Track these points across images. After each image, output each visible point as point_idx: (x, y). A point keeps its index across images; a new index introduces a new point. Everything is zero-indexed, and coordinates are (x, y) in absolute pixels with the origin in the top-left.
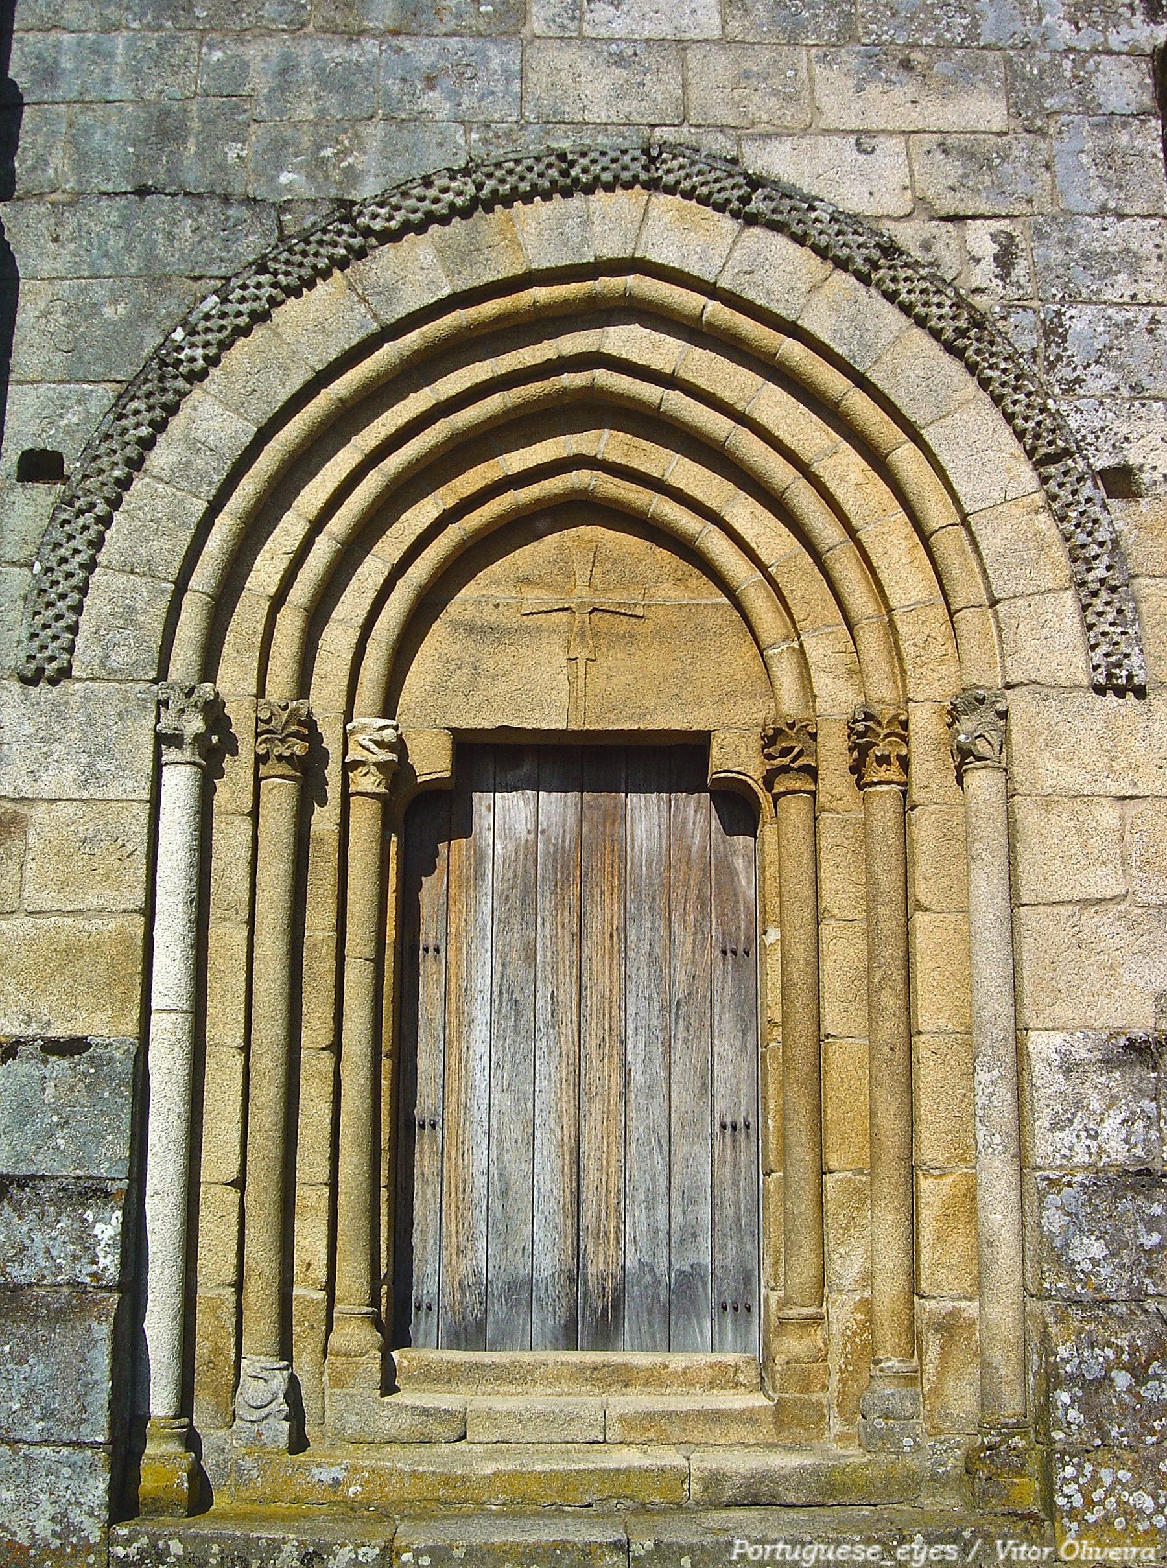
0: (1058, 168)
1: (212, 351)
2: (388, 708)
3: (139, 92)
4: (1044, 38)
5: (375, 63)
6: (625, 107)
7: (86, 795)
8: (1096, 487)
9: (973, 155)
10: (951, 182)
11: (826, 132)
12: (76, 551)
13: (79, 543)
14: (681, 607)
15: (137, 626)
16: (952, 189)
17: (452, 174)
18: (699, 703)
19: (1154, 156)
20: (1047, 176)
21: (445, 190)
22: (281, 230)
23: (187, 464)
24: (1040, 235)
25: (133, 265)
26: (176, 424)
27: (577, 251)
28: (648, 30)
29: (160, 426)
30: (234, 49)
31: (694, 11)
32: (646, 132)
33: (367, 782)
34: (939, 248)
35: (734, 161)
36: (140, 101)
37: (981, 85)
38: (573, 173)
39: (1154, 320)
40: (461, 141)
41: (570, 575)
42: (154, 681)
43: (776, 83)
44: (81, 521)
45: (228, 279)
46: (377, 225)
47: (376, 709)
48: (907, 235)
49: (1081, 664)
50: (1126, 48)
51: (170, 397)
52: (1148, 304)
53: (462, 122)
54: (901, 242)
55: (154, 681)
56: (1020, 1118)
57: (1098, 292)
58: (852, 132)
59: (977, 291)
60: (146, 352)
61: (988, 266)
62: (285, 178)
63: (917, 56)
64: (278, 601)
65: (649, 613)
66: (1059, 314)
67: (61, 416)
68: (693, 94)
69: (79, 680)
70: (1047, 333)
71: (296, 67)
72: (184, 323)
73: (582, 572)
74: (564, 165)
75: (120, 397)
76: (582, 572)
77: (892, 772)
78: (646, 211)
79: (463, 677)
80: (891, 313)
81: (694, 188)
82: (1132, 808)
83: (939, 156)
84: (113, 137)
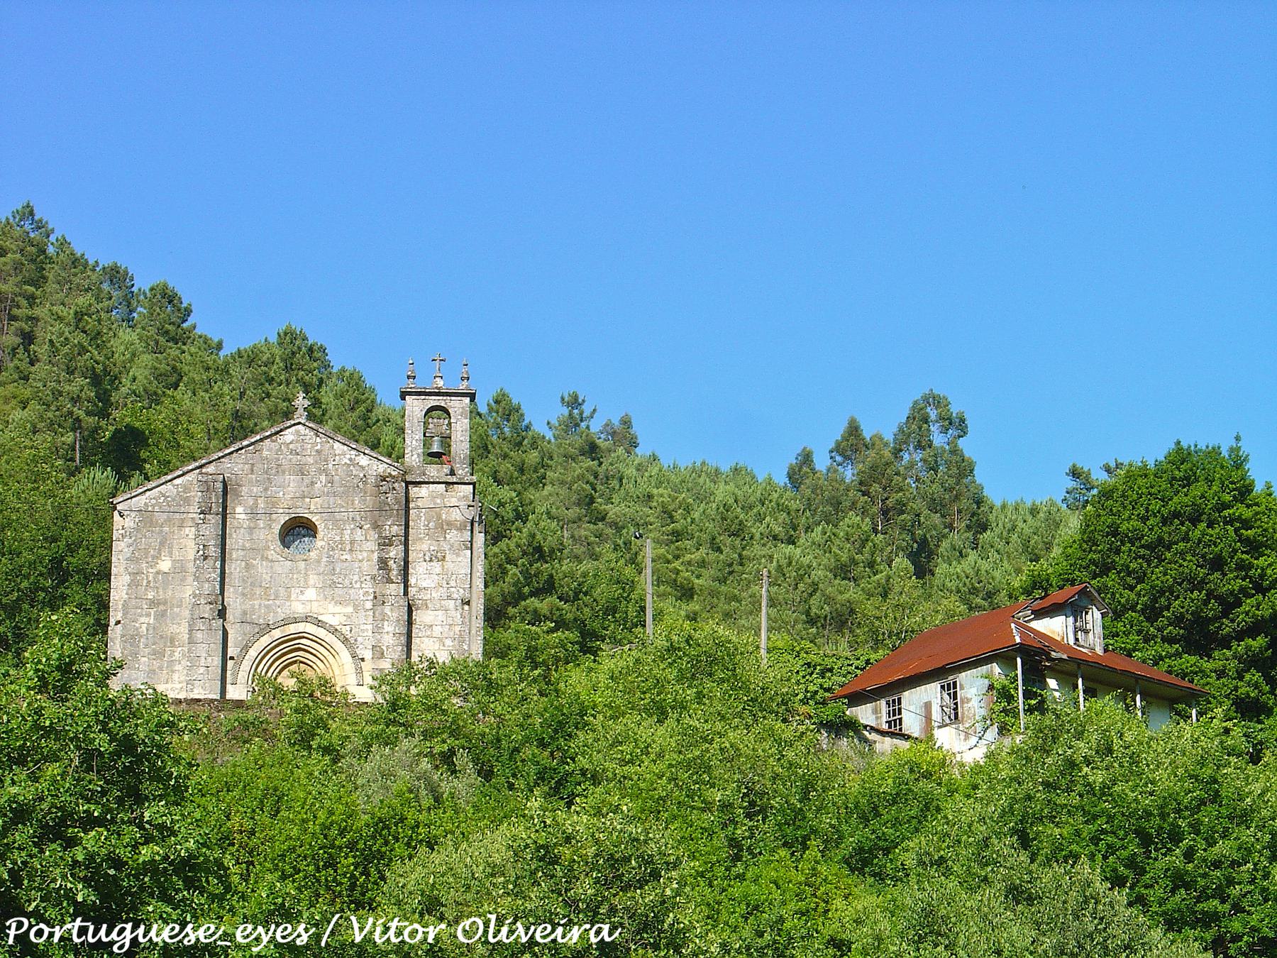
56: (224, 537)
84: (238, 613)
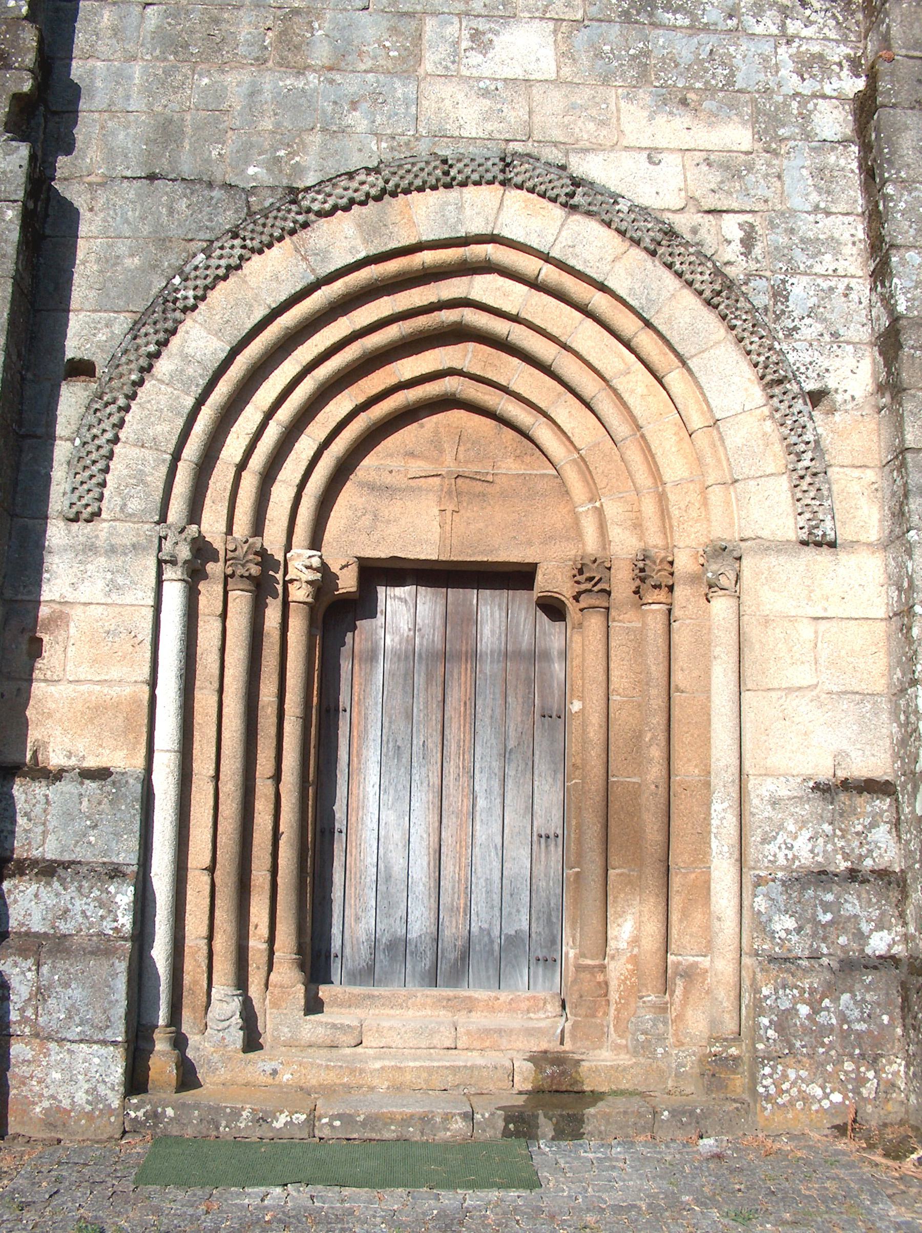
1: (200, 293)
2: (316, 543)
3: (150, 105)
4: (780, 85)
5: (315, 90)
6: (489, 127)
7: (109, 601)
8: (805, 404)
9: (731, 168)
10: (713, 186)
11: (627, 148)
12: (104, 431)
13: (107, 425)
14: (519, 475)
15: (146, 484)
16: (713, 191)
17: (368, 170)
18: (530, 543)
19: (852, 171)
22: (249, 208)
24: (772, 226)
25: (146, 230)
26: (175, 341)
27: (453, 228)
30: (216, 76)
33: (300, 594)
34: (703, 233)
35: (563, 168)
36: (151, 112)
37: (735, 118)
38: (452, 174)
39: (849, 288)
40: (375, 148)
41: (441, 451)
42: (158, 523)
43: (594, 112)
44: (108, 410)
45: (212, 242)
46: (316, 207)
47: (306, 543)
48: (682, 223)
49: (792, 526)
50: (835, 94)
51: (169, 325)
52: (845, 276)
53: (376, 134)
54: (677, 228)
55: (158, 523)
57: (811, 266)
59: (728, 263)
60: (154, 291)
61: (737, 247)
62: (251, 171)
63: (691, 96)
64: (242, 466)
66: (784, 282)
67: (94, 335)
68: (536, 119)
69: (105, 520)
70: (775, 295)
71: (260, 92)
74: (446, 167)
75: (135, 323)
77: (662, 595)
78: (501, 203)
79: (366, 521)
80: (668, 278)
81: (535, 186)
82: (823, 625)
83: (704, 168)
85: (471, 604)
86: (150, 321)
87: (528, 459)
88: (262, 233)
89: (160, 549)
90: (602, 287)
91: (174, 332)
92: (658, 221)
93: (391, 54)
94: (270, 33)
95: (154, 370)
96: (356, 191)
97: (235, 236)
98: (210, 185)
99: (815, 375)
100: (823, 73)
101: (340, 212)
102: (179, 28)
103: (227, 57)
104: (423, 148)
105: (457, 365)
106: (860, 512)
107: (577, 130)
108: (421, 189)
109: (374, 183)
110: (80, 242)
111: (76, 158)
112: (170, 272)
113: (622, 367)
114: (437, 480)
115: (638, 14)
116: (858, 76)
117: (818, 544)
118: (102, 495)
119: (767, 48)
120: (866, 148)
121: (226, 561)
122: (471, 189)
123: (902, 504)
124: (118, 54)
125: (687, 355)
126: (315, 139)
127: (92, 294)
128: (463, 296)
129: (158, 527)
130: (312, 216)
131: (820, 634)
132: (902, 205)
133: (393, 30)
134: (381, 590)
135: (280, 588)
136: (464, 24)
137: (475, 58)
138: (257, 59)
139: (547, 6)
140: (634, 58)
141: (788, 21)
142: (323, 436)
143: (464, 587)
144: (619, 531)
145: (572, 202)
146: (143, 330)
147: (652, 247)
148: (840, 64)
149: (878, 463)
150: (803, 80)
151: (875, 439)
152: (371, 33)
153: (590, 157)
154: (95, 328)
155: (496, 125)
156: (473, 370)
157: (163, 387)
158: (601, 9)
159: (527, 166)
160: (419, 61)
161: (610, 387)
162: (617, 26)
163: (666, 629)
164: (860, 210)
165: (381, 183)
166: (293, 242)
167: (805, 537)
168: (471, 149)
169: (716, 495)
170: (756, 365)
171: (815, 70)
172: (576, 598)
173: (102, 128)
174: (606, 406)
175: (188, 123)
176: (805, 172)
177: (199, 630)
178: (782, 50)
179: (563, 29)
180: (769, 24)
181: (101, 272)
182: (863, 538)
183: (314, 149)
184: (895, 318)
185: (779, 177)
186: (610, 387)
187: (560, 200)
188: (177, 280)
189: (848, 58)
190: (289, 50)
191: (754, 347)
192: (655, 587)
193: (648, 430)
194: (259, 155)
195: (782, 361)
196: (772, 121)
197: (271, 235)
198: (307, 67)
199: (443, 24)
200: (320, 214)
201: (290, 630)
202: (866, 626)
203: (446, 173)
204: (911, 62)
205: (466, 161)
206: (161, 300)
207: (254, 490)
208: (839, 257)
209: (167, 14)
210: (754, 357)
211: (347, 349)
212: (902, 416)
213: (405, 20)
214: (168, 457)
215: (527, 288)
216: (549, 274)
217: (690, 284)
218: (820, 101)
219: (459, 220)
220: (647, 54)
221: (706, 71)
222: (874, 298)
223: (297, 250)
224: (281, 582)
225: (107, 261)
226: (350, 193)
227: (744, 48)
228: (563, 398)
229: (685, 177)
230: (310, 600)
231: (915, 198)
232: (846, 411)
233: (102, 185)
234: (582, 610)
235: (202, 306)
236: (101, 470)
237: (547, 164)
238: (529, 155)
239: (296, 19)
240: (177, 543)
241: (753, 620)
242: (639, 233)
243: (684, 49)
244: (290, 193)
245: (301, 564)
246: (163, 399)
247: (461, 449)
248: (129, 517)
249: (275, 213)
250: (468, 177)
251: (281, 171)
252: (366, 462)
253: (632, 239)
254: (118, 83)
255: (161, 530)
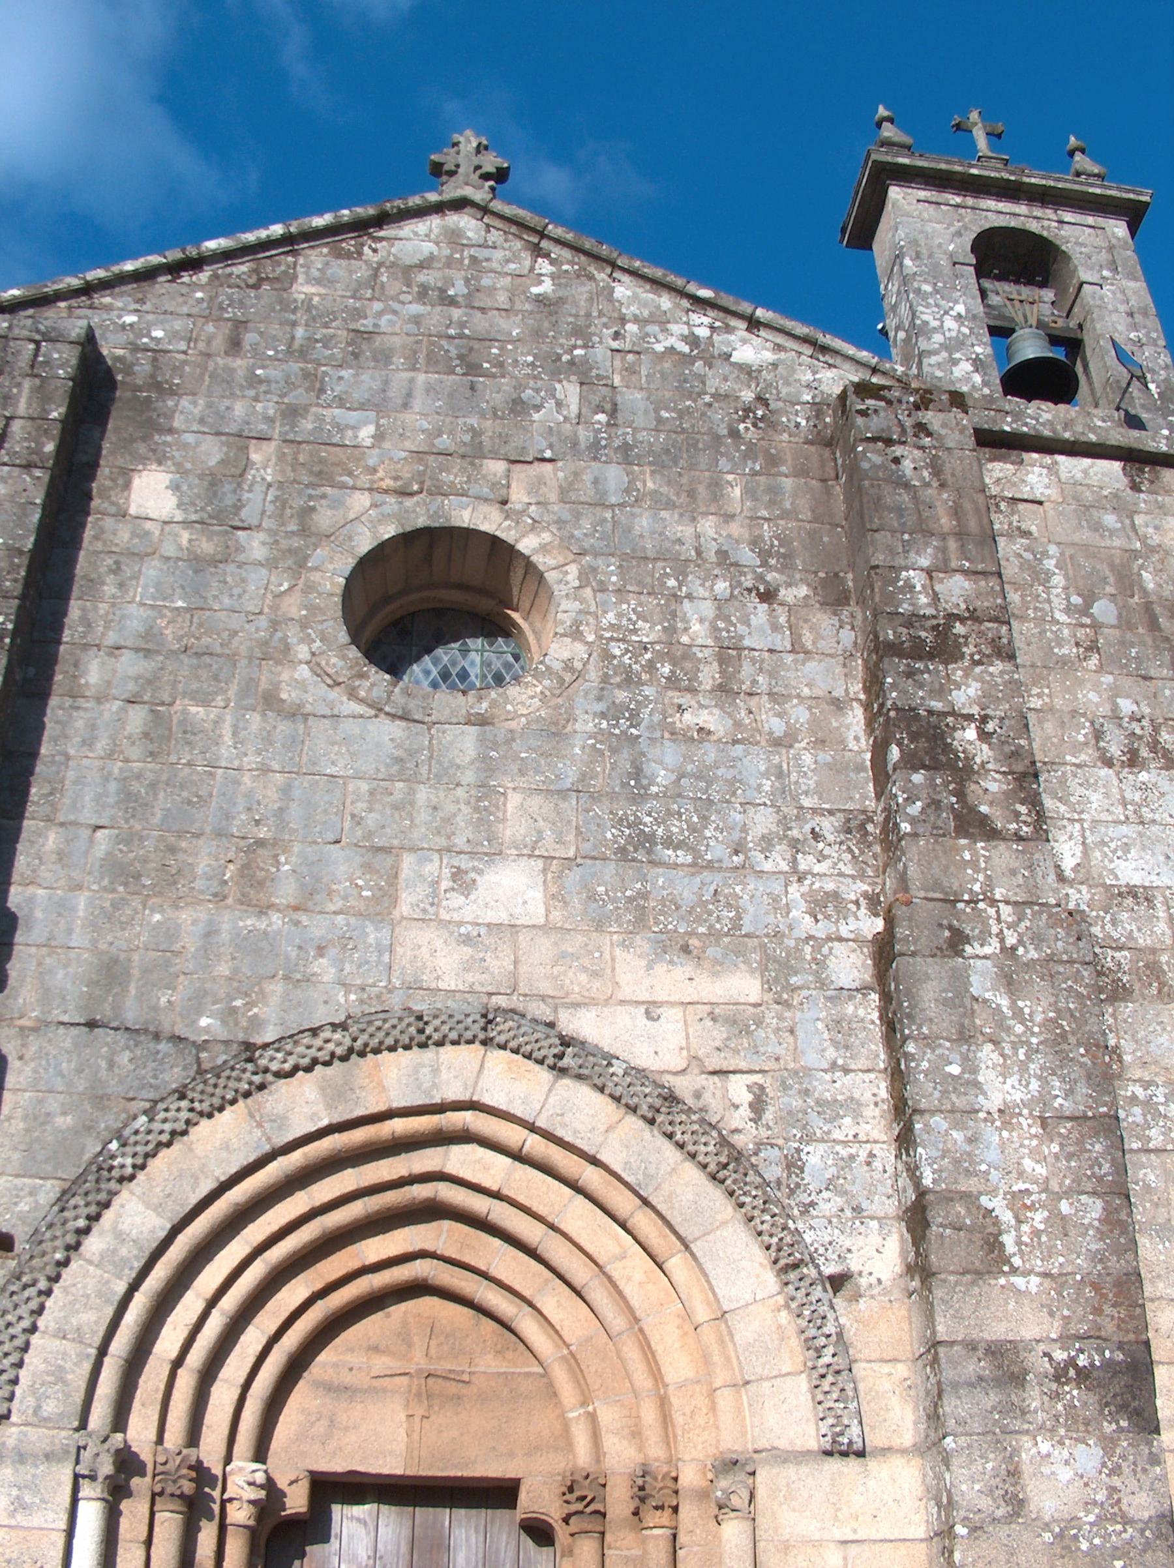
0: (800, 1033)
1: (139, 1161)
2: (260, 1453)
3: (94, 942)
4: (791, 927)
5: (279, 932)
6: (470, 977)
7: (13, 1522)
8: (825, 1290)
9: (737, 1022)
10: (718, 1043)
11: (622, 1002)
12: (20, 1318)
13: (23, 1311)
14: (499, 1374)
15: (65, 1383)
16: (718, 1049)
17: (334, 1026)
18: (511, 1455)
19: (873, 1022)
20: (791, 1039)
21: (327, 1041)
22: (199, 1065)
23: (115, 1251)
24: (785, 1087)
25: (81, 1085)
26: (108, 1216)
27: (428, 1093)
28: (490, 917)
29: (95, 1218)
30: (170, 913)
31: (525, 902)
32: (485, 999)
33: (239, 1514)
34: (707, 1098)
35: (551, 1025)
36: (94, 949)
37: (742, 966)
38: (428, 1032)
39: (871, 1155)
40: (342, 1000)
41: (410, 1345)
42: (77, 1430)
43: (586, 962)
44: (27, 1293)
45: (156, 1102)
46: (274, 1066)
47: (250, 1454)
48: (683, 1086)
49: (813, 1433)
50: (852, 936)
51: (103, 1196)
52: (867, 1142)
53: (344, 985)
54: (678, 1092)
55: (77, 1430)
57: (829, 1132)
58: (643, 1003)
59: (736, 1131)
60: (88, 1156)
61: (745, 1112)
62: (204, 1022)
63: (694, 942)
64: (178, 1363)
65: (474, 1379)
66: (798, 1150)
67: (16, 1204)
68: (523, 969)
69: (14, 1425)
70: (788, 1167)
71: (217, 932)
72: (119, 1137)
73: (419, 1342)
74: (421, 1024)
75: (64, 1192)
76: (419, 1342)
77: (665, 1517)
78: (482, 1066)
79: (321, 1428)
80: (668, 1149)
81: (520, 1046)
82: (853, 1550)
83: (708, 1023)
85: (443, 1526)
86: (81, 1191)
87: (510, 1355)
88: (213, 1095)
89: (77, 1462)
90: (594, 1161)
91: (107, 1205)
92: (656, 1084)
93: (364, 893)
94: (231, 866)
95: (82, 1248)
96: (320, 1049)
97: (182, 1097)
98: (157, 1036)
99: (835, 1257)
100: (838, 912)
101: (301, 1073)
102: (131, 855)
103: (183, 891)
104: (395, 1002)
105: (429, 1246)
106: (891, 1414)
107: (568, 982)
108: (392, 1049)
109: (339, 1041)
110: (6, 1095)
111: (8, 998)
112: (106, 1135)
113: (617, 1250)
114: (404, 1380)
115: (636, 850)
116: (876, 915)
117: (844, 1454)
118: (13, 1394)
119: (777, 887)
120: (886, 998)
121: (154, 1476)
122: (448, 1049)
123: (936, 1405)
124: (62, 882)
125: (690, 1238)
126: (276, 989)
127: (16, 1156)
128: (437, 1169)
129: (77, 1435)
130: (269, 1077)
131: (850, 1561)
132: (925, 1065)
133: (367, 867)
134: (336, 1509)
135: (216, 1508)
136: (445, 861)
137: (457, 900)
138: (215, 895)
139: (536, 842)
140: (631, 900)
141: (800, 856)
142: (273, 1327)
143: (434, 1506)
144: (616, 1440)
145: (560, 1064)
146: (72, 1202)
147: (650, 1115)
148: (857, 903)
149: (910, 1355)
150: (817, 921)
151: (906, 1327)
152: (342, 870)
153: (582, 1012)
154: (17, 1196)
155: (478, 976)
156: (447, 1253)
157: (91, 1268)
158: (595, 847)
159: (511, 1023)
160: (395, 901)
161: (604, 1273)
162: (612, 865)
163: (671, 1558)
164: (882, 1066)
165: (348, 1042)
166: (247, 1106)
167: (828, 1447)
168: (449, 1003)
169: (725, 1399)
170: (768, 1248)
171: (830, 910)
172: (566, 1520)
173: (40, 964)
174: (599, 1295)
175: (135, 964)
176: (820, 1025)
177: (119, 1559)
178: (793, 888)
179: (553, 868)
180: (778, 861)
181: (27, 1130)
182: (896, 1442)
183: (274, 1000)
184: (922, 1193)
185: (792, 1032)
186: (604, 1273)
187: (547, 1062)
188: (114, 1146)
189: (865, 895)
190: (251, 886)
191: (765, 1227)
192: (656, 1508)
193: (648, 1324)
194: (214, 1003)
195: (798, 1243)
196: (782, 968)
197: (223, 1098)
198: (271, 906)
199: (422, 861)
200: (279, 1075)
201: (227, 1559)
202: (903, 1549)
203: (421, 1031)
204: (930, 905)
205: (444, 1017)
206: (94, 1168)
207: (191, 1392)
208: (860, 1120)
209: (118, 840)
210: (766, 1238)
211: (304, 1228)
212: (932, 1304)
213: (381, 856)
214: (93, 1352)
215: (509, 1160)
216: (534, 1145)
217: (693, 1156)
218: (836, 944)
219: (434, 1085)
220: (644, 895)
221: (710, 914)
222: (900, 1167)
223: (251, 1116)
224: (218, 1501)
225: (35, 1119)
226: (313, 1052)
227: (751, 887)
228: (550, 1286)
229: (687, 1035)
230: (252, 1522)
231: (939, 1056)
232: (872, 1297)
233: (35, 1030)
234: (572, 1535)
235: (141, 1176)
236: (13, 1365)
237: (535, 1021)
238: (513, 1011)
239: (260, 851)
240: (97, 1455)
241: (771, 1547)
242: (636, 1100)
243: (686, 889)
244: (246, 1050)
245: (242, 1482)
246: (91, 1284)
247: (433, 1343)
248: (44, 1422)
249: (228, 1073)
250: (445, 1036)
251: (236, 1024)
252: (322, 1357)
253: (627, 1106)
254: (60, 915)
255: (80, 1438)
